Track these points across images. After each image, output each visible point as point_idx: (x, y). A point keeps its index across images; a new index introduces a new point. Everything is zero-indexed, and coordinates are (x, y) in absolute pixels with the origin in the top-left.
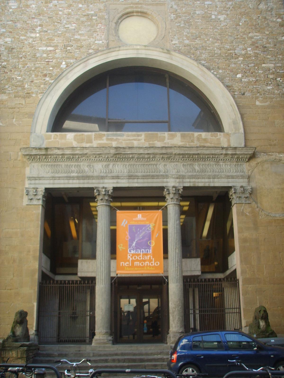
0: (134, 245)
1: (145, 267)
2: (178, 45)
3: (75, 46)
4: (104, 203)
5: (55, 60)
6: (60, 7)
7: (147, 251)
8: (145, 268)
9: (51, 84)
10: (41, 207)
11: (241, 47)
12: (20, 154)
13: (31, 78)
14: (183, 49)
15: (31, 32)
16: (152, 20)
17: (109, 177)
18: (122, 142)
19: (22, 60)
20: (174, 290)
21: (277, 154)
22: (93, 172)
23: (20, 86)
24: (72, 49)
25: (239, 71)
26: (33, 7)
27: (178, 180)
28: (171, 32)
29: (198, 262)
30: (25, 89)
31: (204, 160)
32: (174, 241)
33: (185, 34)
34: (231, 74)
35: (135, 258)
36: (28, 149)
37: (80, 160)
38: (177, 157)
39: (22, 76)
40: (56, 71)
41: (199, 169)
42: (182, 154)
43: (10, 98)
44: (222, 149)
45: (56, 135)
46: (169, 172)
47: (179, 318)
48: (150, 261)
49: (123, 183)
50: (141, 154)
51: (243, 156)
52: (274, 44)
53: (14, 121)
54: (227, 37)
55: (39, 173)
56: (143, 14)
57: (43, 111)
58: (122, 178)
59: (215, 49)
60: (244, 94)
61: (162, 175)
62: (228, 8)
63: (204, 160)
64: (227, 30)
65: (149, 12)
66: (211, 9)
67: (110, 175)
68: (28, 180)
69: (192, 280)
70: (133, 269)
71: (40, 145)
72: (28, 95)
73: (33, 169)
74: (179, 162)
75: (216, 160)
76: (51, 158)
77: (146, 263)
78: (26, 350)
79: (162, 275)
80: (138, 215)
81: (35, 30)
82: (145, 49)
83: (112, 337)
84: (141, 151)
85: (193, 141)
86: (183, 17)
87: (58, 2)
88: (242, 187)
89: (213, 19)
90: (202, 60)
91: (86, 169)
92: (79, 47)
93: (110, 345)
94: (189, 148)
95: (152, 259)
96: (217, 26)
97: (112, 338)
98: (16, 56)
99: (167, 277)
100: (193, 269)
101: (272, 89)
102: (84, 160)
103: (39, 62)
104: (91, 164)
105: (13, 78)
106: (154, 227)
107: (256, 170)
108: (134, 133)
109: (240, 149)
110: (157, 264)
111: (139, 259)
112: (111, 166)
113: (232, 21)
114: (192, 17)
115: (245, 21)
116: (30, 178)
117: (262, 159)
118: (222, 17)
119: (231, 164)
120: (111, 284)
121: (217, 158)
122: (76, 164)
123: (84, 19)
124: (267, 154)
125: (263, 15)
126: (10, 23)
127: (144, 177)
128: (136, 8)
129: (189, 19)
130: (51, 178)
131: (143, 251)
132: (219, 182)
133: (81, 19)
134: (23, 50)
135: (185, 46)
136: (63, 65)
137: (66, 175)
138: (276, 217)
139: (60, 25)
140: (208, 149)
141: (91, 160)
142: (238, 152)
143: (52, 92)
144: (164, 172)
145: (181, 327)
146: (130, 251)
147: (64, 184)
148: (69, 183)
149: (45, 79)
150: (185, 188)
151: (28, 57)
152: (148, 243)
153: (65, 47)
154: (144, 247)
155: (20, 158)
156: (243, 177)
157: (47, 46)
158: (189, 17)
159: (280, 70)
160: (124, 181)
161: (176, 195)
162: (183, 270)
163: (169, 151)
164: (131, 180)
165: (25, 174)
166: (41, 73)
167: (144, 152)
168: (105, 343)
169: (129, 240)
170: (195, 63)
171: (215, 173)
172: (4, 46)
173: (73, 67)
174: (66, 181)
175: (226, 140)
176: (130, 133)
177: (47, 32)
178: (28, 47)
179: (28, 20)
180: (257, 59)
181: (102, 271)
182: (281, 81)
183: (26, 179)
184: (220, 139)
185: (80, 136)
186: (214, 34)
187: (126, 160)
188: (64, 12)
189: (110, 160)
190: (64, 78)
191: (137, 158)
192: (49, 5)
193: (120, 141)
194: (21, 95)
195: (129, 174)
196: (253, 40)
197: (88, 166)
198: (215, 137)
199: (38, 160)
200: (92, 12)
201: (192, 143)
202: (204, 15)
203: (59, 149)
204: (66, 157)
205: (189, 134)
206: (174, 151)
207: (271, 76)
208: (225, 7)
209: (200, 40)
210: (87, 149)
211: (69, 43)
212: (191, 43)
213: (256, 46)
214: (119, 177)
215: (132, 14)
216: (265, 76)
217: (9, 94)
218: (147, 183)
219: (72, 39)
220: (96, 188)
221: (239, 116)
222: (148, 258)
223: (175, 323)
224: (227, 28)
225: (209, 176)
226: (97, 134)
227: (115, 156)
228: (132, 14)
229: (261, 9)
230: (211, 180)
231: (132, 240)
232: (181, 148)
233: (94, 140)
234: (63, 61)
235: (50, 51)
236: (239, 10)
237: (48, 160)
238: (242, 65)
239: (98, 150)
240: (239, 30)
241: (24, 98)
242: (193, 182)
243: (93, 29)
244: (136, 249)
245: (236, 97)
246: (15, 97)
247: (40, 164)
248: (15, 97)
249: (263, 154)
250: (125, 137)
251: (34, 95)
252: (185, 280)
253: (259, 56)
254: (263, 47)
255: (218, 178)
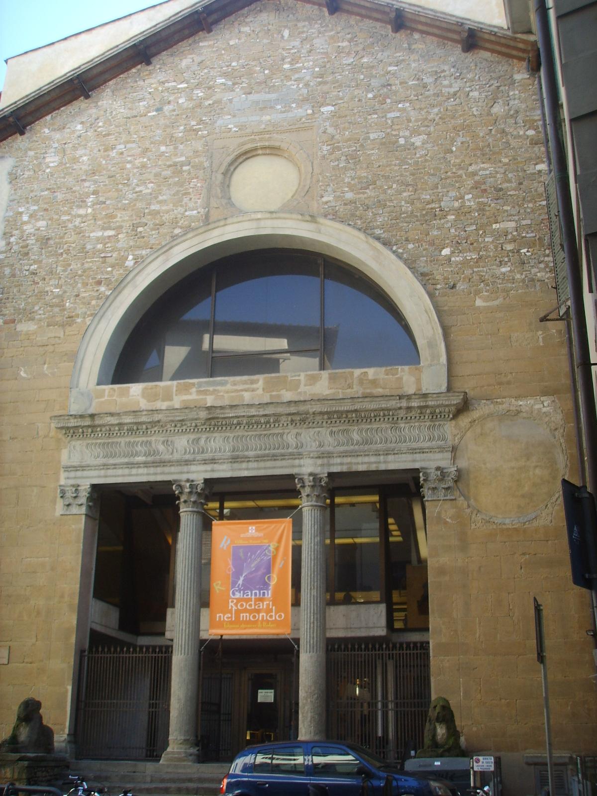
0: (240, 582)
1: (260, 623)
2: (333, 204)
3: (150, 224)
4: (189, 507)
5: (117, 253)
6: (129, 156)
7: (264, 593)
8: (259, 625)
9: (107, 297)
10: (83, 517)
11: (453, 194)
12: (53, 425)
13: (76, 290)
14: (341, 210)
15: (80, 207)
16: (290, 159)
17: (198, 461)
18: (223, 396)
19: (62, 259)
20: (308, 664)
21: (513, 400)
22: (172, 453)
23: (57, 306)
24: (145, 230)
25: (447, 242)
26: (83, 161)
27: (319, 461)
28: (321, 179)
29: (382, 612)
30: (64, 310)
31: (369, 420)
32: (309, 574)
33: (346, 180)
34: (432, 249)
35: (242, 605)
36: (62, 418)
37: (149, 432)
38: (318, 418)
39: (61, 287)
40: (118, 273)
41: (359, 438)
42: (327, 413)
43: (40, 327)
44: (400, 399)
45: (112, 389)
46: (304, 447)
47: (312, 717)
48: (268, 611)
49: (223, 470)
50: (253, 416)
51: (442, 409)
52: (518, 182)
53: (45, 369)
54: (426, 178)
55: (82, 459)
56: (273, 151)
57: (92, 348)
58: (220, 461)
59: (403, 203)
60: (454, 287)
61: (291, 454)
62: (431, 121)
63: (369, 420)
64: (427, 164)
65: (284, 146)
66: (399, 127)
67: (199, 457)
68: (65, 471)
69: (343, 647)
70: (238, 626)
71: (86, 410)
72: (71, 320)
73: (75, 452)
74: (323, 427)
75: (390, 420)
76: (101, 431)
77: (261, 615)
78: (27, 767)
79: (288, 637)
80: (250, 528)
81: (85, 201)
82: (272, 219)
83: (198, 748)
84: (253, 412)
85: (350, 386)
86: (345, 148)
87: (125, 147)
88: (438, 469)
89: (401, 146)
90: (378, 227)
91: (161, 448)
92: (158, 225)
93: (190, 763)
94: (338, 401)
95: (271, 607)
96: (408, 159)
97: (198, 750)
98: (53, 252)
99: (297, 641)
100: (371, 625)
101: (510, 271)
102: (157, 432)
103: (89, 260)
104: (170, 439)
105: (47, 292)
106: (277, 549)
107: (469, 434)
108: (245, 378)
109: (435, 396)
110: (280, 616)
111: (248, 607)
112: (202, 442)
113: (438, 145)
114: (362, 145)
115: (462, 143)
116: (67, 469)
117: (482, 413)
118: (418, 141)
119: (420, 426)
120: (200, 652)
121: (393, 415)
122: (145, 439)
123: (168, 173)
124: (492, 402)
125: (499, 127)
126: (46, 193)
127: (259, 458)
128: (261, 140)
129: (355, 150)
130: (102, 467)
131: (256, 594)
132: (395, 462)
133: (163, 173)
134: (64, 240)
135: (345, 204)
136: (130, 263)
137: (126, 460)
138: (504, 524)
139: (126, 188)
140: (373, 401)
141: (169, 431)
142: (430, 403)
143: (109, 313)
144: (296, 448)
145: (317, 734)
146: (234, 594)
147: (123, 476)
148: (130, 475)
149: (98, 288)
150: (331, 475)
151: (72, 252)
152: (266, 578)
153: (135, 227)
154: (258, 587)
155: (52, 434)
156: (441, 449)
157: (104, 229)
158: (356, 147)
159: (527, 233)
160: (224, 467)
161: (316, 489)
162: (327, 626)
163: (302, 408)
164: (236, 465)
165: (59, 462)
166: (92, 279)
167: (258, 413)
168: (180, 760)
169: (232, 573)
170: (361, 235)
171: (389, 445)
172: (34, 235)
173: (145, 263)
174: (126, 471)
175: (413, 379)
176: (238, 378)
177: (104, 203)
178: (73, 234)
179: (74, 186)
180: (483, 215)
181: (182, 630)
182: (528, 254)
183: (62, 470)
184: (406, 379)
185: (151, 388)
186: (401, 175)
187: (229, 428)
188: (134, 165)
189: (200, 430)
190: (130, 285)
191: (247, 424)
192: (111, 153)
193: (219, 394)
194: (58, 322)
195: (234, 453)
196: (477, 178)
197: (163, 442)
198: (393, 375)
199: (81, 436)
200: (183, 159)
201: (349, 390)
202: (384, 140)
203: (112, 414)
204: (126, 428)
205: (344, 372)
206: (312, 408)
207: (509, 247)
208: (426, 119)
209: (374, 188)
210: (159, 414)
211: (140, 219)
212: (358, 196)
213: (482, 190)
214: (215, 459)
215: (254, 153)
216: (496, 247)
217: (40, 320)
218: (265, 468)
219: (146, 211)
220: (175, 481)
221: (440, 331)
222: (265, 607)
223: (306, 726)
224: (426, 161)
225: (377, 450)
226: (180, 383)
227: (208, 423)
228: (254, 153)
229: (495, 114)
230: (382, 457)
231: (237, 574)
232: (323, 402)
233: (176, 395)
234: (130, 253)
235: (109, 237)
236: (453, 121)
237: (96, 435)
238: (453, 231)
239: (178, 414)
240: (450, 161)
241: (63, 326)
242: (348, 464)
243: (182, 189)
244: (244, 590)
245: (437, 294)
246: (48, 326)
247: (85, 442)
248: (48, 326)
249: (485, 401)
250: (229, 387)
251: (79, 320)
252: (330, 647)
253: (487, 208)
254: (496, 189)
255: (394, 454)
